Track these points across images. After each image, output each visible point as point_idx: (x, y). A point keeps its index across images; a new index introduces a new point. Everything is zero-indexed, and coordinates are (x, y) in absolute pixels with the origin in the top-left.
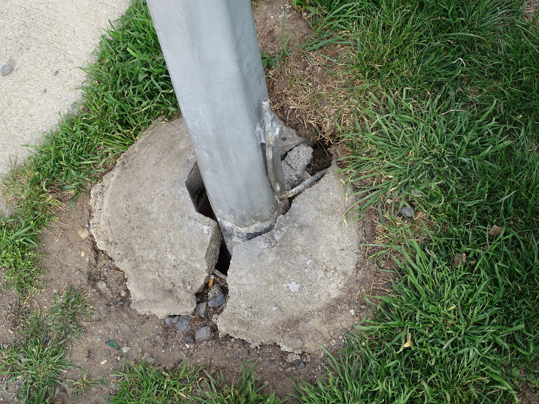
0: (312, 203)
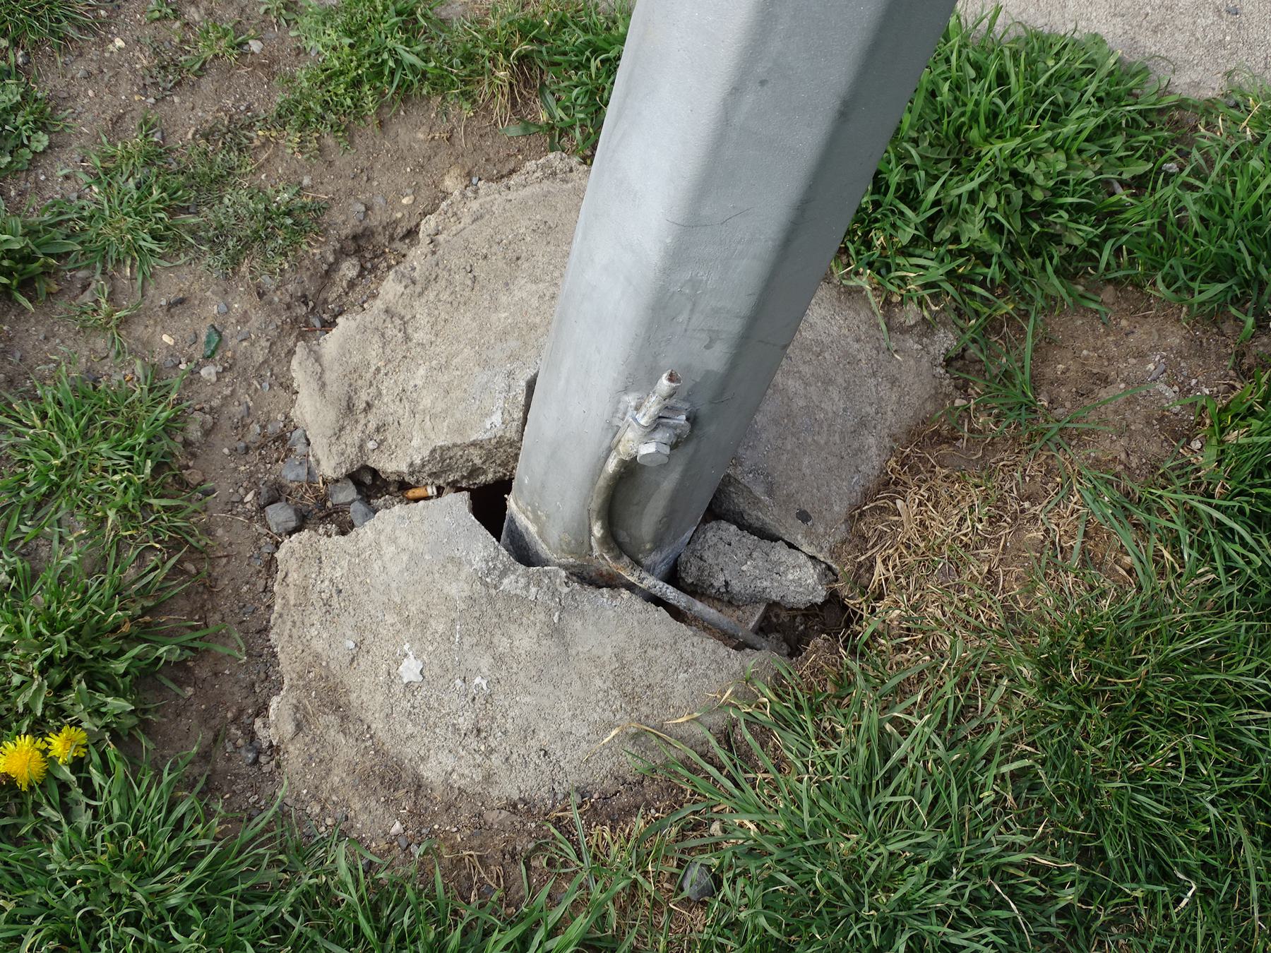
0: (630, 636)
